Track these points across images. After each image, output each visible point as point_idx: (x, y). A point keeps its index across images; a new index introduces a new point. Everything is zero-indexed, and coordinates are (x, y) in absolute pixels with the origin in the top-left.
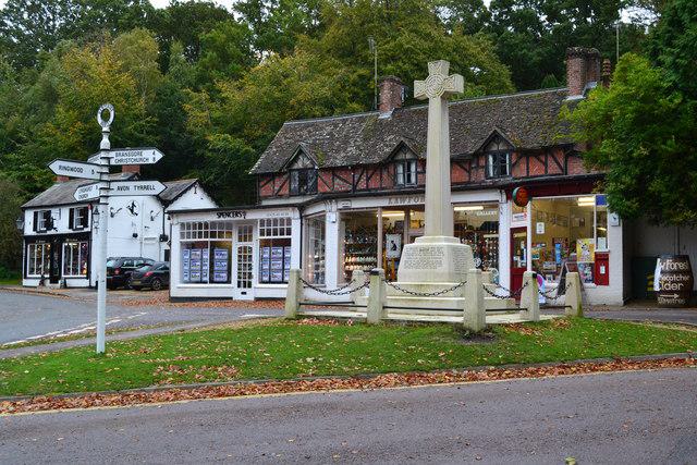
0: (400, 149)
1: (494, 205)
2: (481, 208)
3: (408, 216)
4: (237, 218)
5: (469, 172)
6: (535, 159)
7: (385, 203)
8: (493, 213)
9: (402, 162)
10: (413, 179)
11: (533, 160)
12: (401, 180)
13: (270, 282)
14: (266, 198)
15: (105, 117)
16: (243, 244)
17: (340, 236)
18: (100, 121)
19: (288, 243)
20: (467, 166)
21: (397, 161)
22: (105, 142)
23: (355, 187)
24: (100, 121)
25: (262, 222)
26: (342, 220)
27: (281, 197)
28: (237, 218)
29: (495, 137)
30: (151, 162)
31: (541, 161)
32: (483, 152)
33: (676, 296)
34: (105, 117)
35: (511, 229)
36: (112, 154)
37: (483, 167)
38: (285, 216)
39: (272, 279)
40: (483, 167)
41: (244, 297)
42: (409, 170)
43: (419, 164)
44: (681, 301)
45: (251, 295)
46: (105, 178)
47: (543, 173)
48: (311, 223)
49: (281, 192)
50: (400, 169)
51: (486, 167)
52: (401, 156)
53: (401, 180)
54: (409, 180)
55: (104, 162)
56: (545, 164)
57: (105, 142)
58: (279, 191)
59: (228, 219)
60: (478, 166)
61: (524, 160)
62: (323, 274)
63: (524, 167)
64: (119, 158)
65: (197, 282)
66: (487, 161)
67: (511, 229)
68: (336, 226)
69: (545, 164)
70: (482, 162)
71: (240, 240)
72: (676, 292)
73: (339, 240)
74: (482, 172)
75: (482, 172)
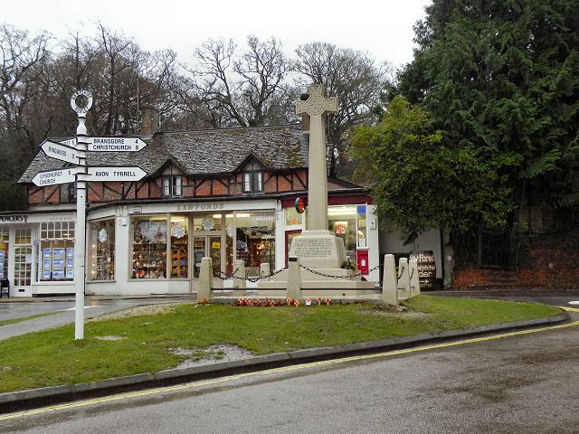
0: (168, 166)
1: (271, 212)
2: (248, 215)
3: (224, 217)
4: (17, 222)
5: (228, 187)
6: (283, 179)
7: (174, 209)
8: (270, 218)
9: (169, 177)
10: (178, 192)
11: (281, 179)
12: (248, 188)
13: (51, 279)
14: (35, 204)
15: (81, 102)
16: (20, 245)
17: (130, 237)
18: (74, 105)
19: (70, 244)
20: (226, 182)
21: (165, 176)
22: (82, 128)
23: (123, 199)
24: (74, 105)
25: (44, 226)
26: (133, 223)
27: (51, 204)
28: (17, 222)
29: (251, 159)
30: (133, 149)
31: (287, 179)
32: (241, 170)
33: (427, 281)
34: (81, 102)
35: (286, 232)
36: (90, 140)
37: (240, 183)
38: (68, 220)
39: (54, 277)
40: (240, 183)
41: (22, 294)
42: (175, 184)
43: (184, 179)
44: (430, 285)
45: (28, 292)
46: (83, 163)
47: (290, 189)
48: (94, 227)
49: (51, 200)
50: (167, 183)
51: (243, 183)
52: (167, 172)
53: (248, 188)
54: (175, 193)
55: (82, 147)
56: (291, 182)
57: (82, 128)
58: (48, 199)
59: (7, 222)
60: (236, 183)
61: (274, 178)
62: (16, 269)
63: (191, 189)
64: (99, 144)
65: (62, 280)
66: (243, 178)
67: (286, 232)
68: (127, 228)
69: (291, 182)
70: (239, 180)
71: (17, 242)
72: (427, 278)
73: (130, 242)
74: (239, 187)
75: (239, 187)
